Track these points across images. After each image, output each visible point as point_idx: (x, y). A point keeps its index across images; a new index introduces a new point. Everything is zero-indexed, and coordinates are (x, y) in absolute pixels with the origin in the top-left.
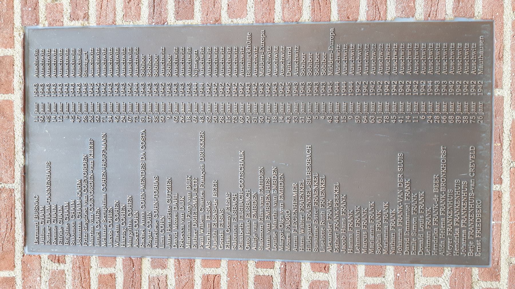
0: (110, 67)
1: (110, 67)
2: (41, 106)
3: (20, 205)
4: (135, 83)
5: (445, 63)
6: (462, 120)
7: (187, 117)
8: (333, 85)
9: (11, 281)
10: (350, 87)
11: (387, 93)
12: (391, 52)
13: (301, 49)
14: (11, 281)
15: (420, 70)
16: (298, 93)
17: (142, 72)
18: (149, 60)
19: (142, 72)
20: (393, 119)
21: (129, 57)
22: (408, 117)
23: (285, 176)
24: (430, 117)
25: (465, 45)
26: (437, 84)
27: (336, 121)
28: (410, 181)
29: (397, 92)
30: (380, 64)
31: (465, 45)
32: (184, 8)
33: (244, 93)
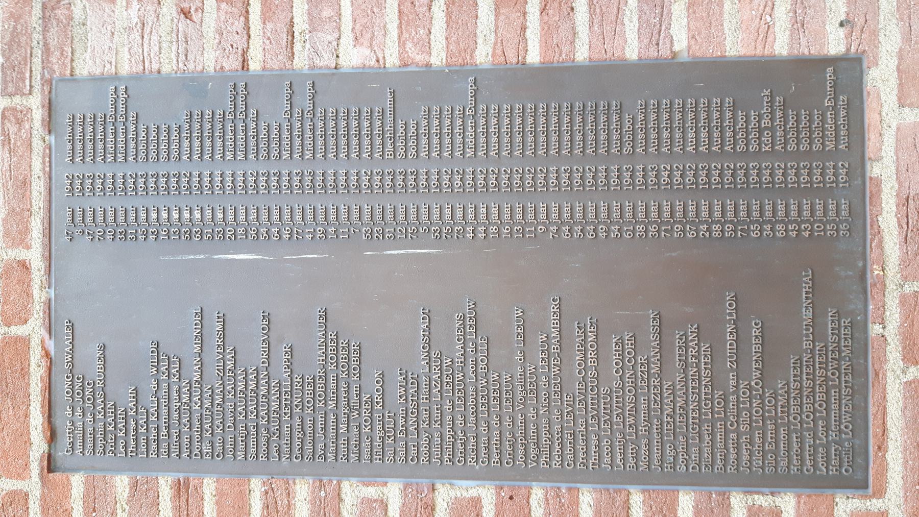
0: (343, 141)
1: (343, 141)
2: (78, 214)
3: (891, 481)
4: (285, 172)
5: (665, 134)
6: (825, 230)
7: (240, 230)
8: (314, 175)
9: (20, 499)
10: (240, 179)
11: (705, 184)
12: (683, 112)
13: (624, 107)
14: (20, 499)
15: (710, 144)
16: (393, 187)
17: (263, 153)
18: (276, 132)
19: (263, 153)
20: (792, 231)
21: (343, 124)
22: (716, 227)
23: (638, 338)
24: (705, 226)
25: (813, 100)
26: (805, 167)
27: (602, 235)
28: (698, 328)
29: (671, 184)
30: (518, 139)
31: (813, 100)
32: (606, 12)
33: (268, 188)
